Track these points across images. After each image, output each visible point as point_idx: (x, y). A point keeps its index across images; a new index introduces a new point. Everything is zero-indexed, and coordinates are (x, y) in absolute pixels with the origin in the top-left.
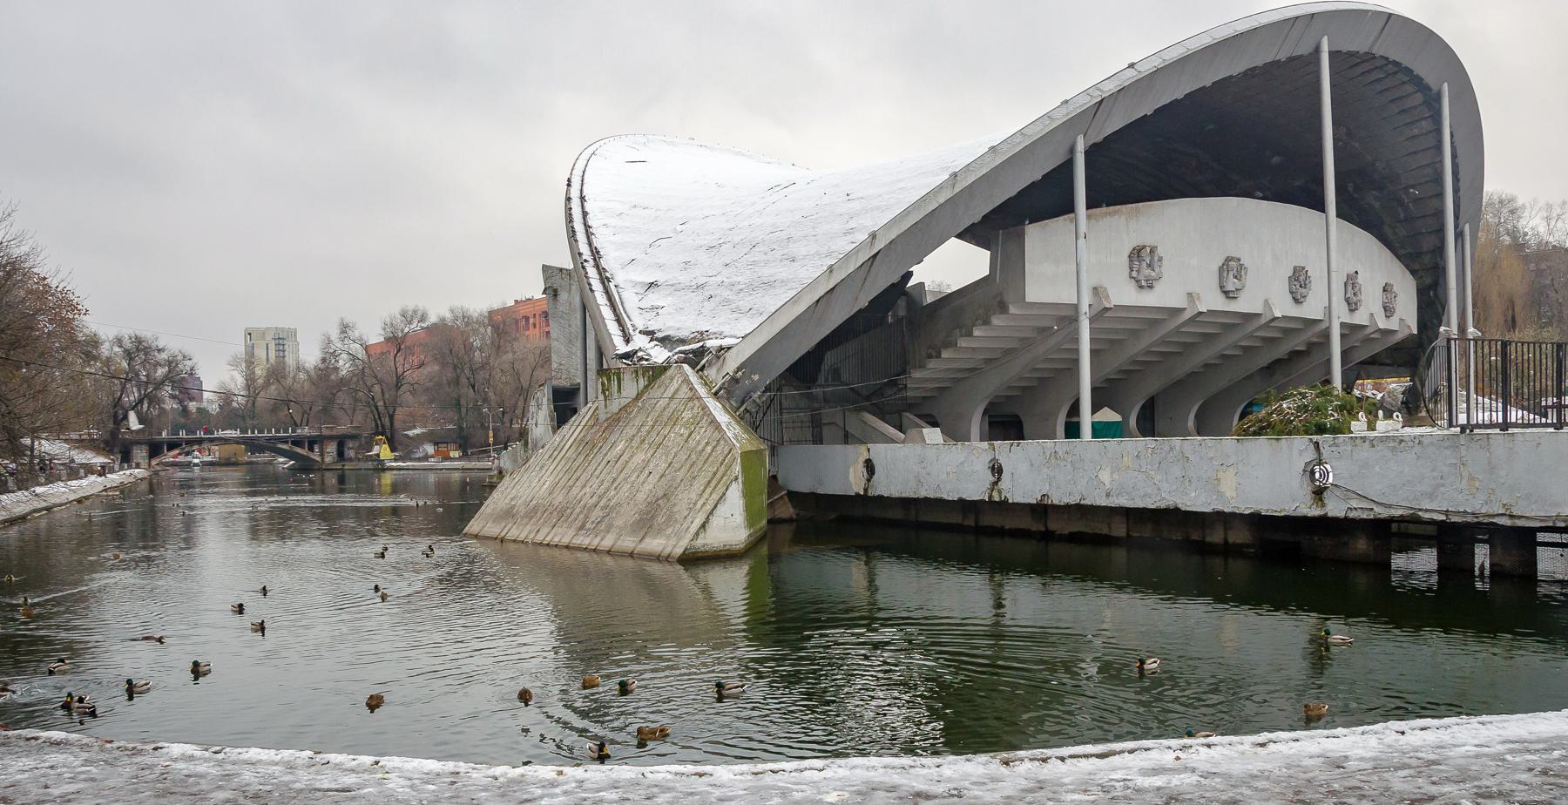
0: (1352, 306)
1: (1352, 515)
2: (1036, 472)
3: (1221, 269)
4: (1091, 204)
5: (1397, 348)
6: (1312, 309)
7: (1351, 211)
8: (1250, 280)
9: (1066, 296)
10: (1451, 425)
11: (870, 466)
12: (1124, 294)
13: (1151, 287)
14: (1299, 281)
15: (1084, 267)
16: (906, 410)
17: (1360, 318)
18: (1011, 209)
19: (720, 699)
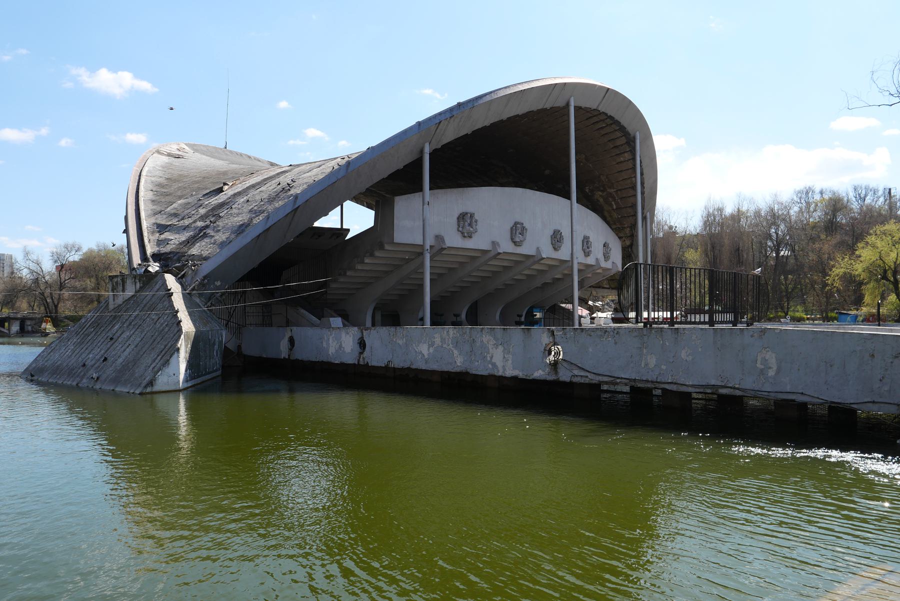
0: (587, 254)
1: (575, 380)
2: (389, 347)
3: (512, 228)
5: (611, 279)
6: (563, 254)
7: (586, 200)
8: (528, 235)
10: (637, 322)
11: (292, 341)
12: (453, 240)
13: (470, 237)
14: (556, 239)
16: (321, 307)
17: (590, 261)
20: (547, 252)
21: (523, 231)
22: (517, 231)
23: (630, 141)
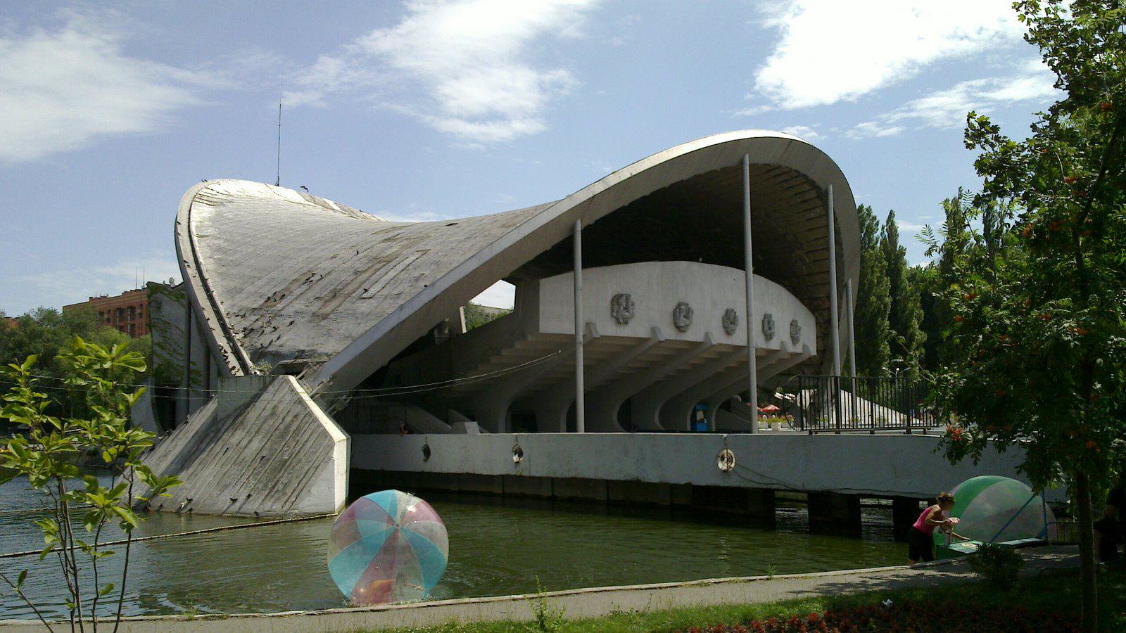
0: (768, 336)
3: (674, 312)
4: (584, 266)
6: (739, 339)
8: (696, 318)
9: (568, 329)
11: (427, 452)
12: (607, 328)
14: (729, 320)
15: (582, 307)
17: (774, 345)
18: (543, 260)
19: (231, 499)
20: (719, 338)
21: (688, 313)
22: (681, 315)
23: (823, 196)
